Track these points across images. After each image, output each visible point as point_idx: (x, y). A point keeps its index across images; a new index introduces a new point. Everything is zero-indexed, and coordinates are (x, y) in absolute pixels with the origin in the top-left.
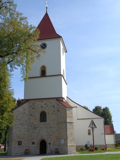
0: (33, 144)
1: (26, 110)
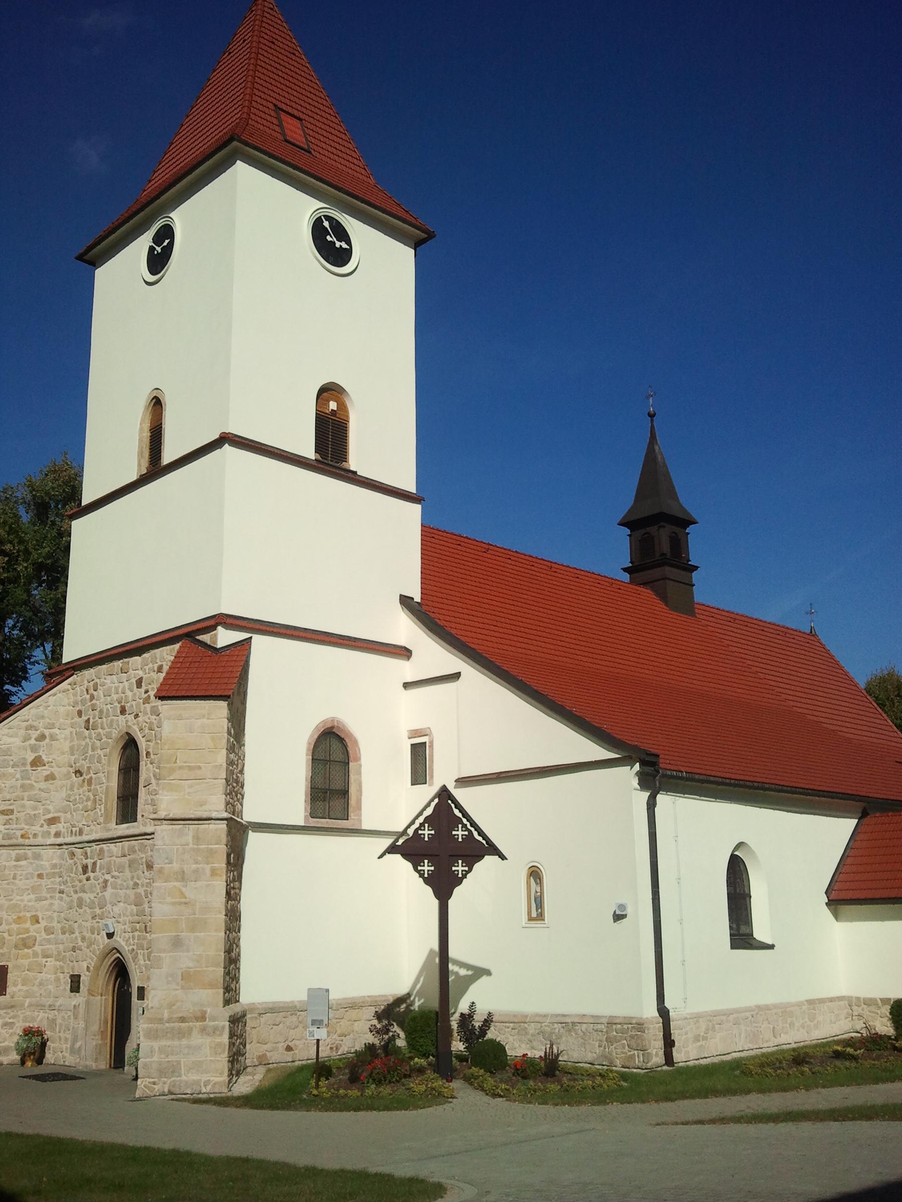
1: (53, 738)
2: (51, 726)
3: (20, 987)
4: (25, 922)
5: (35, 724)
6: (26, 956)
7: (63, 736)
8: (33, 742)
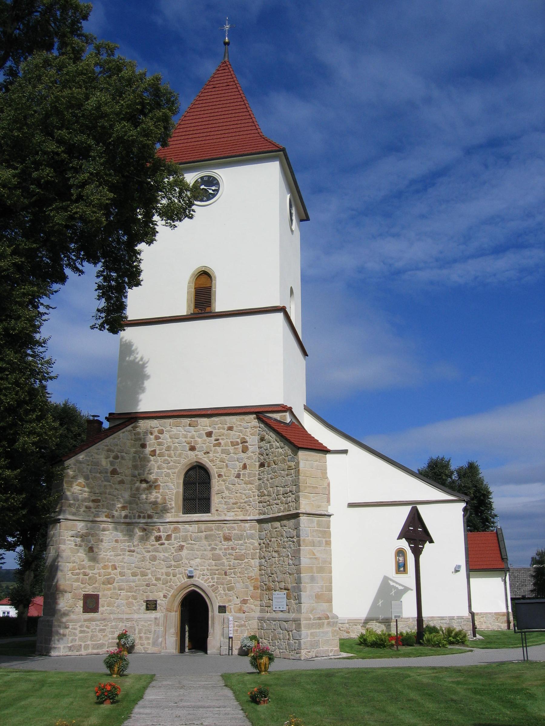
0: (148, 609)
1: (123, 458)
2: (122, 451)
3: (106, 608)
4: (108, 568)
5: (113, 448)
6: (110, 589)
7: (128, 458)
8: (111, 459)
